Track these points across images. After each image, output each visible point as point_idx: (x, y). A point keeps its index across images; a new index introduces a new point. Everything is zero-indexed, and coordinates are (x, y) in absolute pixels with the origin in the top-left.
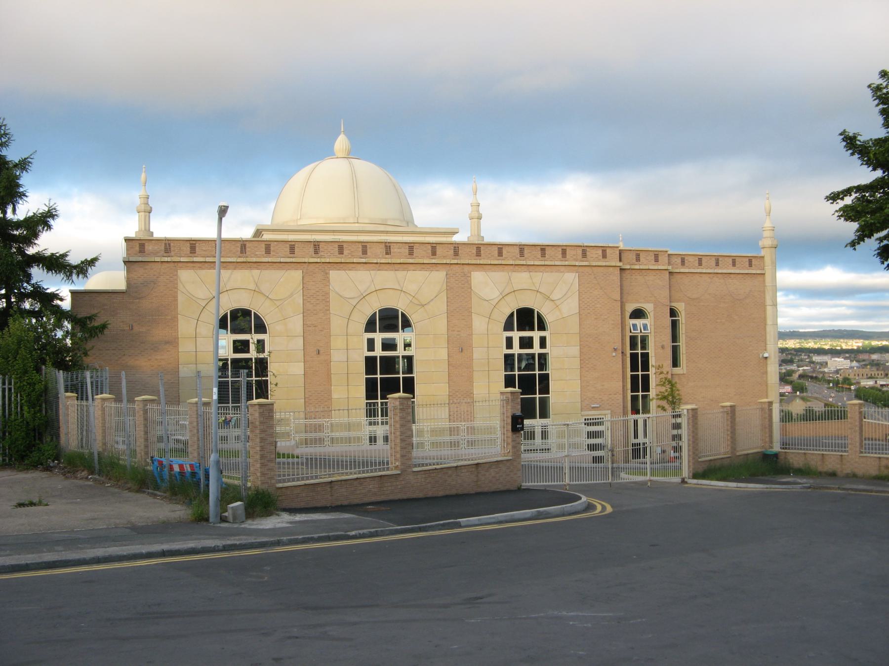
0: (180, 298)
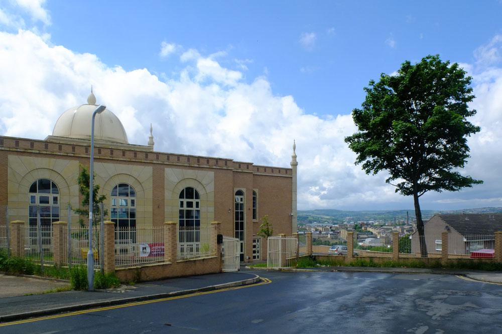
0: (9, 171)
